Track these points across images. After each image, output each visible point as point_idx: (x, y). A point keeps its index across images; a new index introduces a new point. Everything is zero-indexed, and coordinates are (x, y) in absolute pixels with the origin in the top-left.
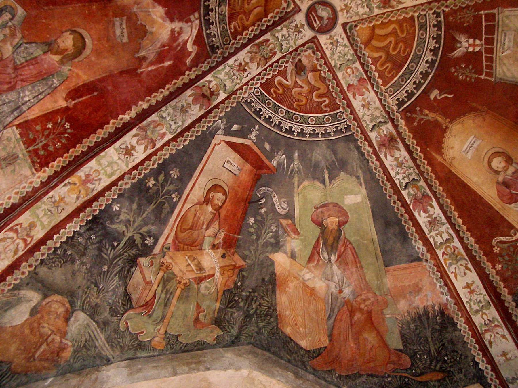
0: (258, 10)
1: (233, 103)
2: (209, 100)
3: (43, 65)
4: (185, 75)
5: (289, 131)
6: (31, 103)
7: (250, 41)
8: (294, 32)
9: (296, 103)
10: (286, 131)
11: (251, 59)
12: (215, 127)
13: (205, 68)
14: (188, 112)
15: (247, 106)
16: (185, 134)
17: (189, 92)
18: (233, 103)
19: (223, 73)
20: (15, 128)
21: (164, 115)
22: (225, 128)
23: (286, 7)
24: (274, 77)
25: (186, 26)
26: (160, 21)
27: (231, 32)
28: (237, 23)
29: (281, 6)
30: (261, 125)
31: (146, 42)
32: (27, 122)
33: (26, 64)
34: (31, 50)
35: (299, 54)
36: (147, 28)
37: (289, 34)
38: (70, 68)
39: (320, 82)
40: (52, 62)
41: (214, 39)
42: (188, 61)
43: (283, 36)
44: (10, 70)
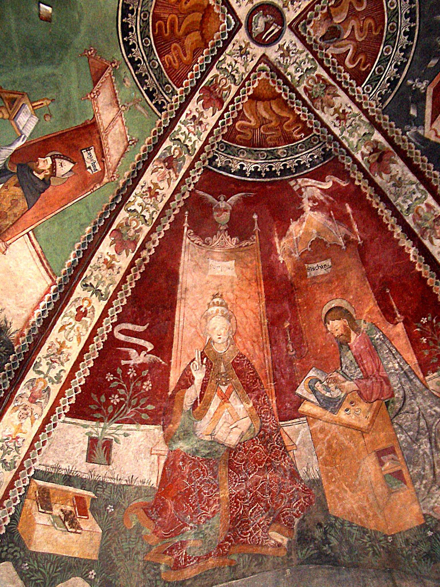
0: (274, 107)
1: (385, 120)
2: (384, 153)
3: (362, 350)
4: (360, 186)
5: (410, 34)
6: (401, 361)
7: (310, 110)
8: (291, 58)
9: (374, 33)
10: (411, 39)
11: (330, 106)
12: (416, 139)
13: (349, 162)
14: (400, 178)
15: (386, 100)
16: (428, 176)
17: (378, 179)
18: (385, 120)
19: (351, 139)
20: (427, 378)
21: (406, 207)
22: (415, 125)
23: (265, 73)
24: (347, 70)
25: (306, 195)
26: (304, 224)
27: (304, 137)
28: (293, 131)
29: (265, 79)
30: (407, 78)
31: (327, 239)
32: (420, 365)
33: (362, 367)
34: (348, 362)
35: (315, 41)
36: (314, 239)
37: (293, 63)
38: (362, 321)
39: (342, 4)
40: (358, 341)
41: (316, 157)
42: (344, 184)
43: (297, 71)
44: (369, 383)
